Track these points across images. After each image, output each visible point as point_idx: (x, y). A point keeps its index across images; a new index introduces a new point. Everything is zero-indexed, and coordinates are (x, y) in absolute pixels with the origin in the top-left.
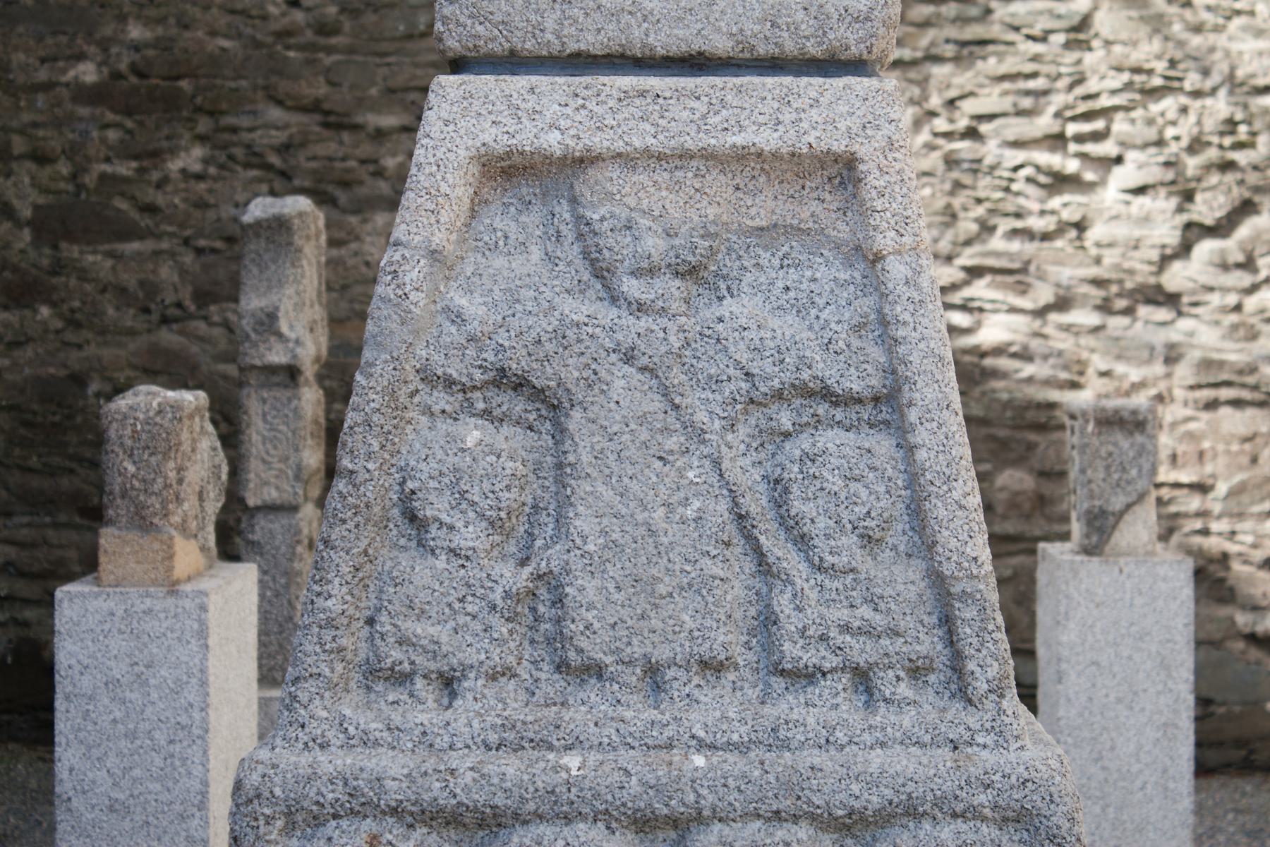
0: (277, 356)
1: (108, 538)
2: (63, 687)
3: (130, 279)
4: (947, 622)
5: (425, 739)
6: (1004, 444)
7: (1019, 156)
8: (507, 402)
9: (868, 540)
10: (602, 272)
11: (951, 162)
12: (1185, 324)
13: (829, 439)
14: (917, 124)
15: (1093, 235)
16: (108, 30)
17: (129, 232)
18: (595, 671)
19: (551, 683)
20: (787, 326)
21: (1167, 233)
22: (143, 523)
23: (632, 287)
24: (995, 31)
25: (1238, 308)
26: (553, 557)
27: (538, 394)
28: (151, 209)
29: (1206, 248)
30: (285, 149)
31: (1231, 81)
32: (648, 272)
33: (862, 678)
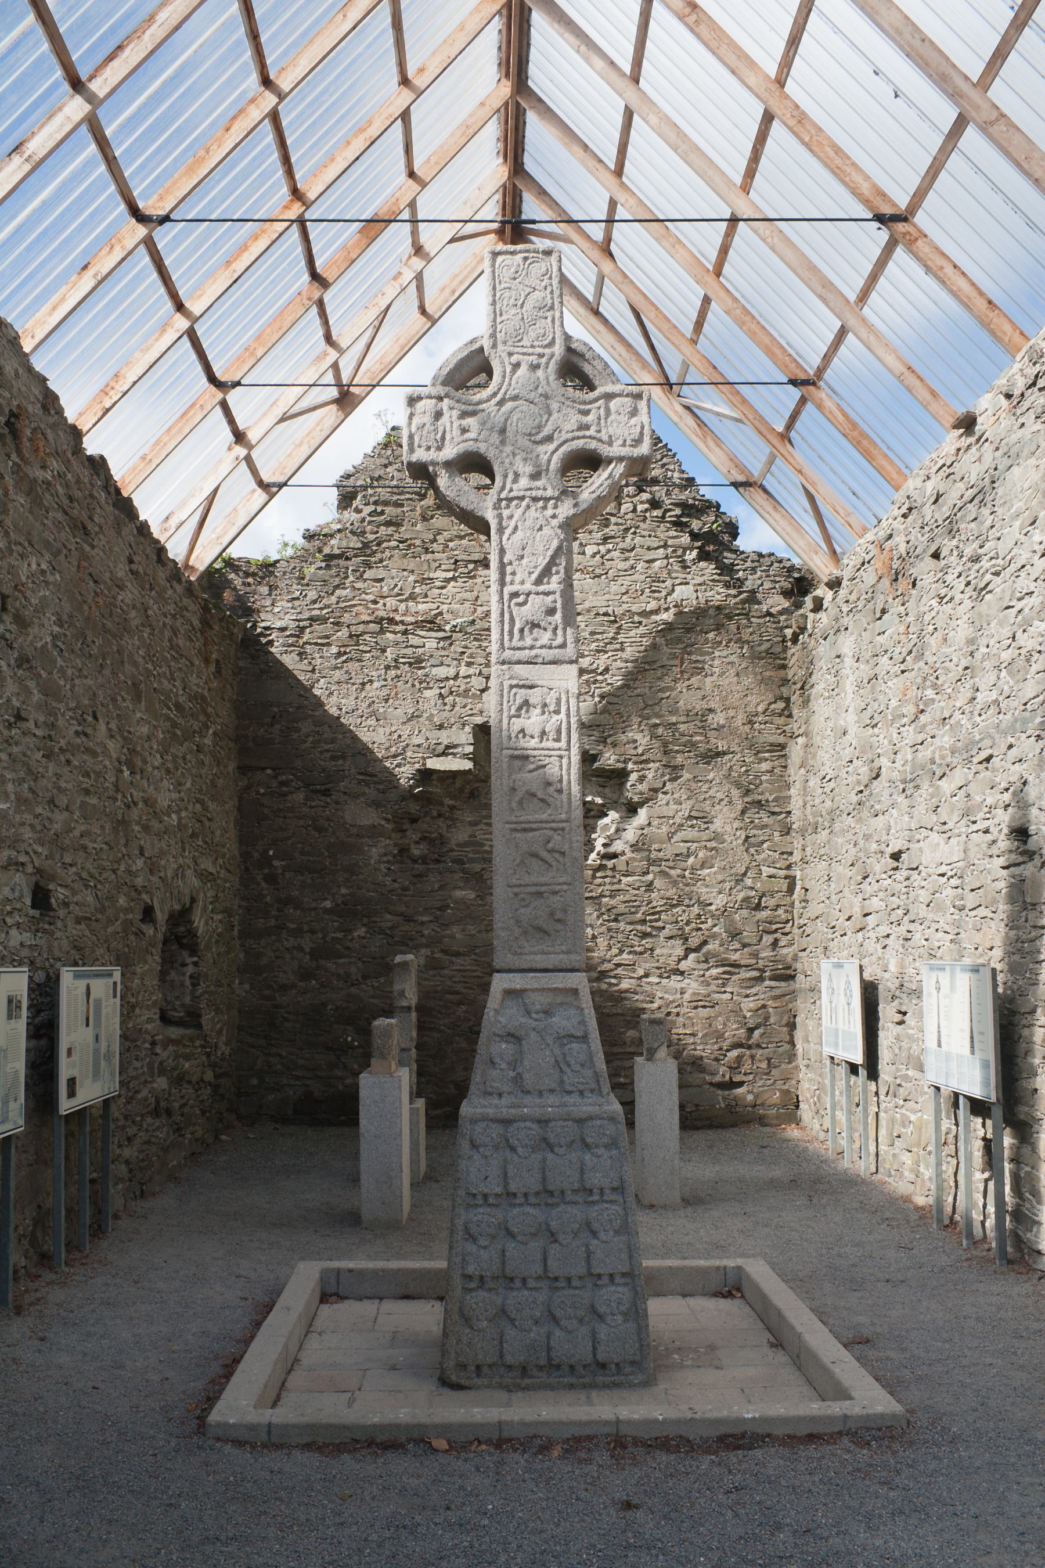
0: (405, 1004)
1: (373, 1061)
2: (362, 1102)
3: (341, 971)
4: (598, 1081)
5: (496, 1106)
6: (629, 1022)
8: (510, 1039)
9: (582, 1065)
10: (528, 1013)
11: (609, 930)
12: (687, 981)
13: (574, 1045)
14: (598, 917)
15: (657, 951)
16: (334, 890)
17: (341, 956)
18: (529, 1092)
19: (520, 1094)
20: (565, 1023)
21: (680, 951)
22: (383, 1057)
23: (534, 1016)
24: (622, 886)
26: (520, 1070)
27: (516, 1037)
28: (348, 948)
29: (692, 956)
30: (391, 928)
31: (699, 902)
32: (537, 1013)
33: (581, 1093)
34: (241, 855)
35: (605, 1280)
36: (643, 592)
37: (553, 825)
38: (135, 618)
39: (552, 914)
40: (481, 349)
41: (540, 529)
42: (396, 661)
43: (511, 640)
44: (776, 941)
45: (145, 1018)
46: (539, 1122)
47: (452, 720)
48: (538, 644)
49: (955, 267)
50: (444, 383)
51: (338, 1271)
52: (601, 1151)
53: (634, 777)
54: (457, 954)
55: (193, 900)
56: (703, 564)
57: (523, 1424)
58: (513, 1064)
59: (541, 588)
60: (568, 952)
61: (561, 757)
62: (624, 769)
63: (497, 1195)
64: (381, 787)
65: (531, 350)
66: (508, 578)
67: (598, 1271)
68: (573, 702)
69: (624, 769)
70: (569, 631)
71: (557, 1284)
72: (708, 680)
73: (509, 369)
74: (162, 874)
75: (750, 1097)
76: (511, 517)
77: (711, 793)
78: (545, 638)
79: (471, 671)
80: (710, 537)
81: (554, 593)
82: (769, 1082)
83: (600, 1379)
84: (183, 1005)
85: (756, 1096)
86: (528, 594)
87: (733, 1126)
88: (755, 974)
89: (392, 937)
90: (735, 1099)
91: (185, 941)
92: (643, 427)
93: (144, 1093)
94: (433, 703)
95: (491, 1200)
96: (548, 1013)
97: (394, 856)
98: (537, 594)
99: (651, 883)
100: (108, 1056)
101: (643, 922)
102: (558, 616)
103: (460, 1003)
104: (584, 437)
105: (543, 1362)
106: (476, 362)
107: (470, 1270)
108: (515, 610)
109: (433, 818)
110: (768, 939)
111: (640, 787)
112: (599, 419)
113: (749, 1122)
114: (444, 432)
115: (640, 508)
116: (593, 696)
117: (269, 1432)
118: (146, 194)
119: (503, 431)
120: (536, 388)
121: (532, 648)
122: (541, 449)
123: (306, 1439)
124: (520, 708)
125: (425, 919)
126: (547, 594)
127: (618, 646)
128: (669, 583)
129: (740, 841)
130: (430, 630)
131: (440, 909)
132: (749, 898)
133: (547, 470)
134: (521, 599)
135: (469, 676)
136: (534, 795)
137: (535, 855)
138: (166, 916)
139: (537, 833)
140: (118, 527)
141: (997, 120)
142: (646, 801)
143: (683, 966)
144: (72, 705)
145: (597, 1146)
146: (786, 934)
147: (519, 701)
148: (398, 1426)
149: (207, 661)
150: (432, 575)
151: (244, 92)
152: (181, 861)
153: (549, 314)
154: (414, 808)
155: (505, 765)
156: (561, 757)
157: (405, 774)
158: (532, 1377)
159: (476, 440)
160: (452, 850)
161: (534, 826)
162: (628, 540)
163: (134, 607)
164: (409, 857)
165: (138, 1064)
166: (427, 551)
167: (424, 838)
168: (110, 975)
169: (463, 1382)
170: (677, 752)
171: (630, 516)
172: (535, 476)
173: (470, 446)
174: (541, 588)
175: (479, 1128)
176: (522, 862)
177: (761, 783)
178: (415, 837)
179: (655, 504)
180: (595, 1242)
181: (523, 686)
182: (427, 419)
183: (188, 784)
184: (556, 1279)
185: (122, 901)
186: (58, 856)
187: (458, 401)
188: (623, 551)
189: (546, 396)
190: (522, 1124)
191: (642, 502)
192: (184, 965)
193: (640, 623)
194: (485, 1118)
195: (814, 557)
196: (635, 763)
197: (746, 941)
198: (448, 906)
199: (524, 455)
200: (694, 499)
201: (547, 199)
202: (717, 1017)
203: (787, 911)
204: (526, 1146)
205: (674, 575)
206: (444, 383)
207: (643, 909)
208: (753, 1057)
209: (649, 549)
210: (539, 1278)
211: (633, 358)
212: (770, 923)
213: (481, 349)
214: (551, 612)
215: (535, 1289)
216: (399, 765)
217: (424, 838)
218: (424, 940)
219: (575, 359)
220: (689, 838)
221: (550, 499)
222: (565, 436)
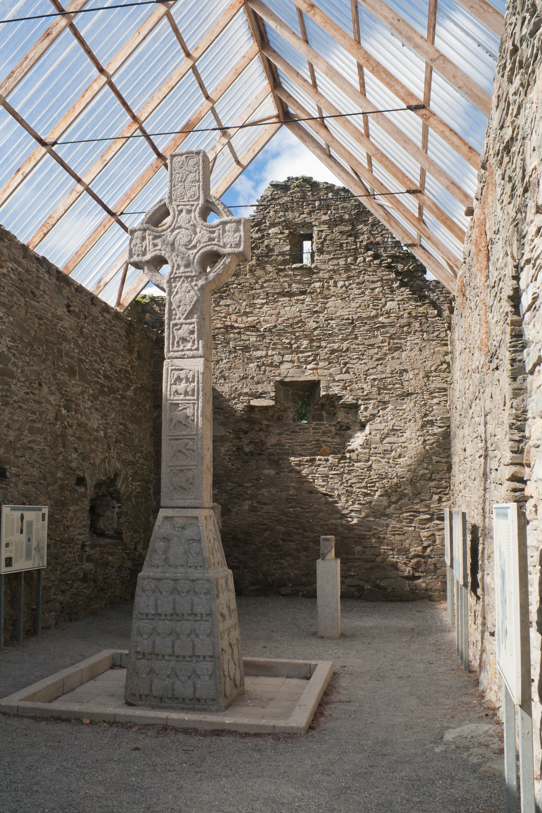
5: (155, 572)
7: (360, 490)
11: (347, 491)
14: (341, 485)
18: (171, 566)
21: (385, 503)
24: (355, 468)
25: (399, 517)
30: (231, 490)
33: (196, 567)
34: (155, 452)
35: (201, 658)
36: (369, 306)
37: (189, 437)
38: (70, 334)
39: (188, 480)
40: (165, 204)
41: (189, 292)
42: (235, 348)
43: (173, 347)
44: (440, 498)
45: (77, 533)
46: (174, 580)
47: (264, 379)
48: (185, 349)
49: (451, 130)
50: (147, 223)
51: (121, 655)
52: (202, 596)
53: (362, 407)
54: (265, 504)
55: (116, 475)
56: (402, 289)
57: (125, 716)
58: (165, 552)
59: (188, 321)
60: (195, 499)
61: (194, 404)
62: (357, 403)
63: (153, 615)
64: (226, 415)
65: (187, 203)
66: (173, 317)
67: (198, 654)
68: (200, 376)
69: (357, 403)
70: (200, 342)
71: (179, 659)
72: (404, 354)
73: (177, 213)
74: (92, 462)
75: (424, 585)
76: (175, 287)
77: (404, 416)
78: (189, 345)
79: (274, 353)
80: (408, 273)
81: (194, 323)
82: (435, 577)
83: (197, 706)
84: (113, 528)
85: (427, 584)
86: (182, 324)
87: (413, 600)
88: (428, 516)
89: (231, 494)
90: (415, 585)
91: (114, 495)
92: (240, 237)
93: (76, 569)
94: (254, 370)
95: (150, 617)
96: (183, 528)
97: (233, 452)
98: (186, 324)
99: (371, 466)
100: (38, 549)
101: (366, 487)
102: (195, 335)
103: (266, 530)
104: (211, 245)
105: (170, 696)
106: (164, 209)
107: (139, 649)
108: (175, 332)
109: (256, 431)
110: (436, 497)
111: (365, 413)
112: (219, 235)
113: (423, 599)
114: (146, 247)
115: (368, 259)
116: (340, 364)
117: (18, 710)
118: (44, 133)
119: (173, 244)
120: (190, 222)
121: (182, 350)
122: (190, 252)
123: (33, 715)
124: (176, 380)
125: (249, 485)
126: (190, 324)
127: (353, 336)
128: (383, 300)
129: (420, 443)
130: (252, 331)
131: (256, 480)
132: (425, 474)
133: (193, 262)
134: (178, 327)
135: (273, 355)
136: (181, 422)
137: (180, 451)
138: (94, 483)
139: (182, 441)
140: (59, 291)
141: (438, 58)
142: (368, 421)
143: (388, 511)
144: (22, 379)
145: (200, 593)
146: (446, 494)
147: (175, 377)
148: (71, 712)
149: (130, 352)
150: (255, 302)
151: (91, 77)
152: (107, 454)
153: (197, 184)
154: (245, 426)
155: (168, 408)
156: (194, 404)
157: (240, 407)
158: (165, 702)
159: (160, 250)
160: (268, 448)
161: (180, 437)
162: (361, 278)
163: (71, 329)
164: (243, 452)
165: (70, 555)
166: (252, 289)
167: (251, 442)
168: (40, 510)
169: (133, 702)
170: (386, 394)
171: (361, 264)
172: (187, 266)
173: (158, 253)
174: (188, 321)
175: (145, 582)
176: (174, 455)
177: (433, 410)
178: (246, 442)
179: (376, 256)
180: (198, 640)
181: (178, 370)
182: (138, 241)
183: (113, 416)
184: (178, 656)
185: (60, 474)
186: (12, 452)
187: (153, 231)
188: (358, 284)
189: (194, 226)
190: (166, 581)
191: (368, 256)
192: (114, 508)
193: (366, 323)
194: (148, 578)
195: (451, 283)
196: (362, 400)
197: (423, 498)
198: (261, 479)
199: (182, 255)
200: (400, 253)
201: (291, 100)
202: (405, 540)
203: (446, 482)
204: (167, 591)
205: (387, 296)
206: (147, 223)
207: (366, 480)
208: (426, 563)
209: (373, 282)
210: (170, 655)
211: (350, 179)
212: (437, 488)
213: (165, 204)
214: (192, 332)
215: (169, 660)
216: (236, 404)
217: (251, 442)
218: (248, 496)
219: (210, 206)
220: (392, 441)
221: (194, 276)
222: (202, 245)
